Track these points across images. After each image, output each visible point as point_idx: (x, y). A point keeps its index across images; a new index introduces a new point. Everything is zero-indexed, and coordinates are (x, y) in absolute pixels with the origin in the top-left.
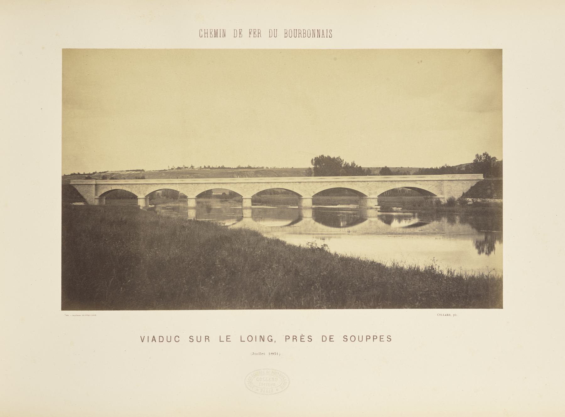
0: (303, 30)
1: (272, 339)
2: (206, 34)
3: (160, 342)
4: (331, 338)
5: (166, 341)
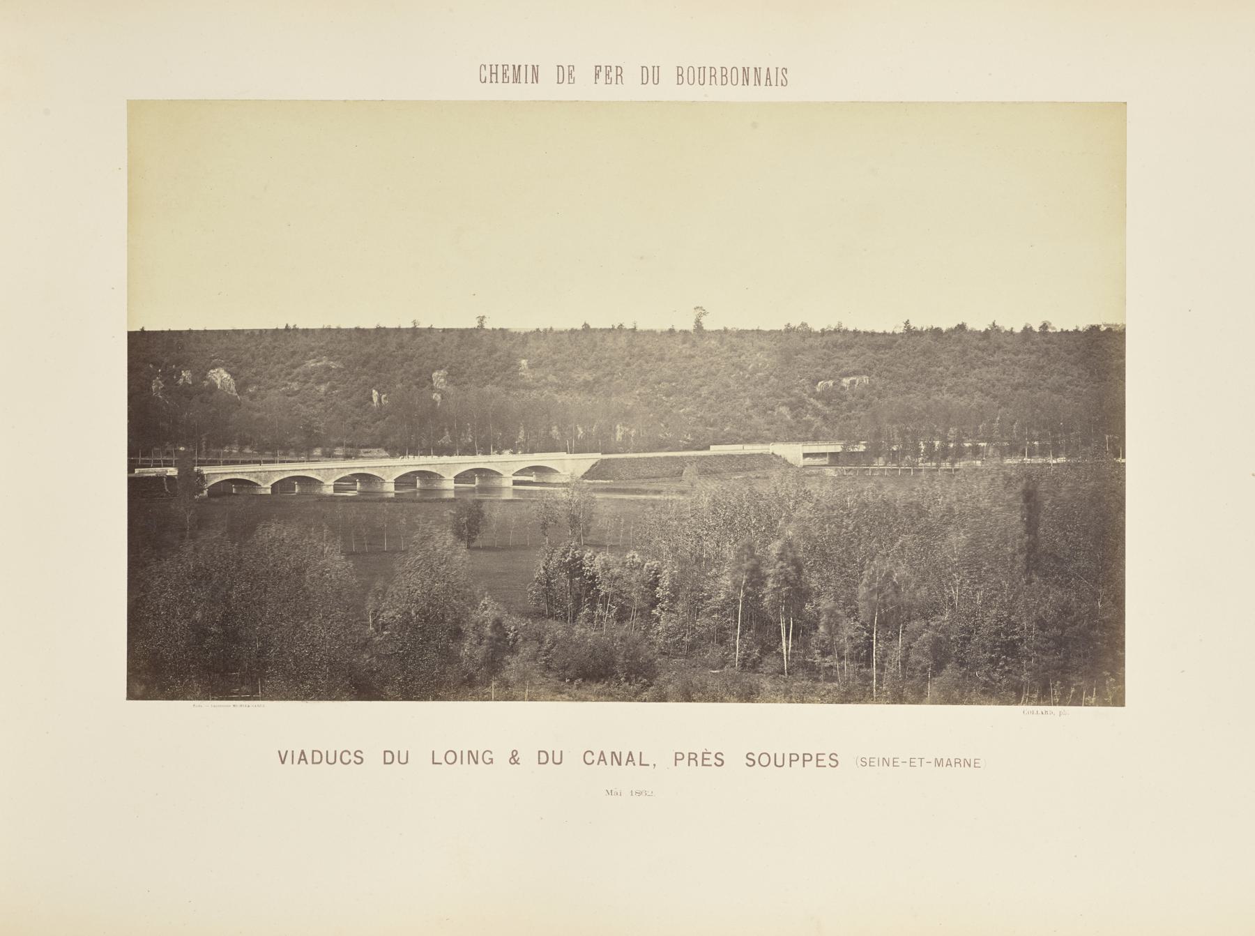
0: (617, 67)
1: (492, 759)
2: (494, 76)
3: (539, 763)
4: (706, 759)
5: (810, 762)
